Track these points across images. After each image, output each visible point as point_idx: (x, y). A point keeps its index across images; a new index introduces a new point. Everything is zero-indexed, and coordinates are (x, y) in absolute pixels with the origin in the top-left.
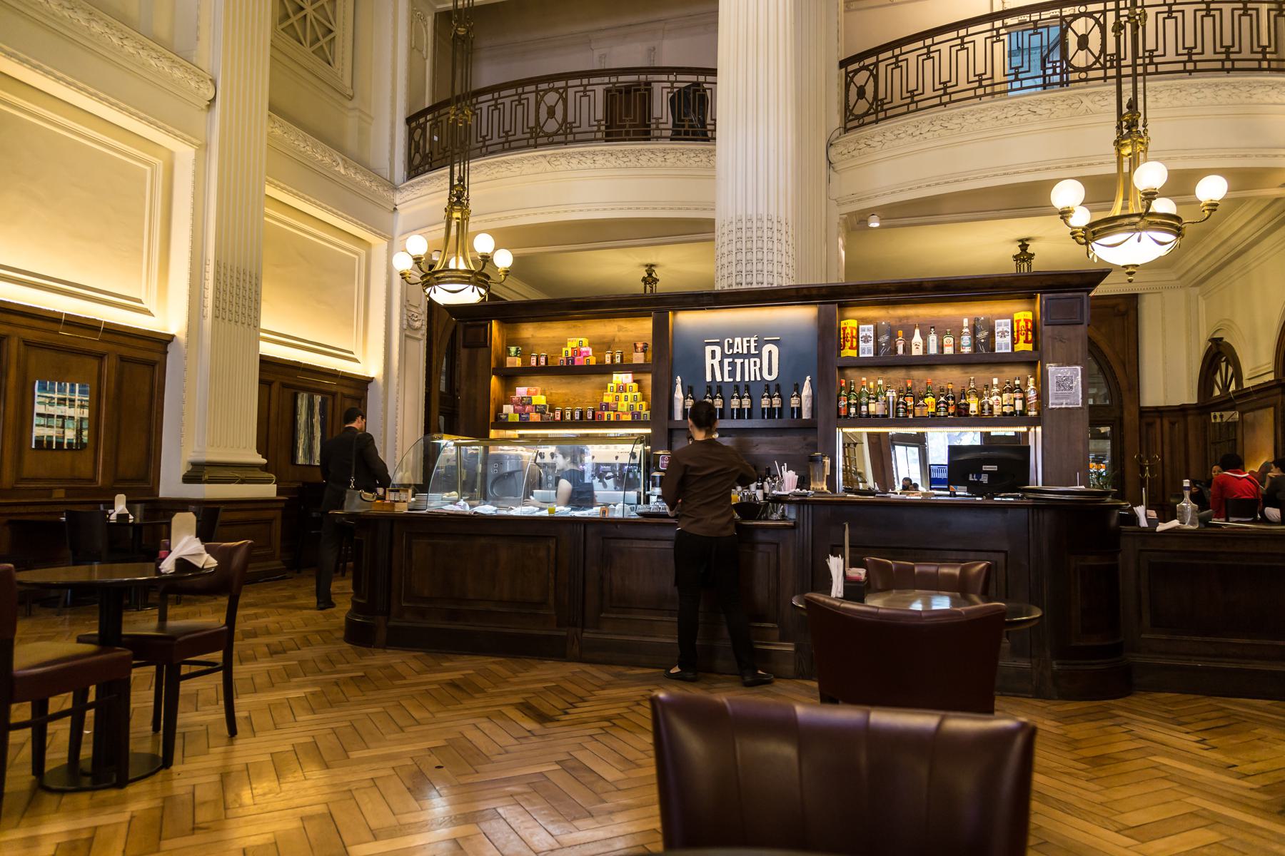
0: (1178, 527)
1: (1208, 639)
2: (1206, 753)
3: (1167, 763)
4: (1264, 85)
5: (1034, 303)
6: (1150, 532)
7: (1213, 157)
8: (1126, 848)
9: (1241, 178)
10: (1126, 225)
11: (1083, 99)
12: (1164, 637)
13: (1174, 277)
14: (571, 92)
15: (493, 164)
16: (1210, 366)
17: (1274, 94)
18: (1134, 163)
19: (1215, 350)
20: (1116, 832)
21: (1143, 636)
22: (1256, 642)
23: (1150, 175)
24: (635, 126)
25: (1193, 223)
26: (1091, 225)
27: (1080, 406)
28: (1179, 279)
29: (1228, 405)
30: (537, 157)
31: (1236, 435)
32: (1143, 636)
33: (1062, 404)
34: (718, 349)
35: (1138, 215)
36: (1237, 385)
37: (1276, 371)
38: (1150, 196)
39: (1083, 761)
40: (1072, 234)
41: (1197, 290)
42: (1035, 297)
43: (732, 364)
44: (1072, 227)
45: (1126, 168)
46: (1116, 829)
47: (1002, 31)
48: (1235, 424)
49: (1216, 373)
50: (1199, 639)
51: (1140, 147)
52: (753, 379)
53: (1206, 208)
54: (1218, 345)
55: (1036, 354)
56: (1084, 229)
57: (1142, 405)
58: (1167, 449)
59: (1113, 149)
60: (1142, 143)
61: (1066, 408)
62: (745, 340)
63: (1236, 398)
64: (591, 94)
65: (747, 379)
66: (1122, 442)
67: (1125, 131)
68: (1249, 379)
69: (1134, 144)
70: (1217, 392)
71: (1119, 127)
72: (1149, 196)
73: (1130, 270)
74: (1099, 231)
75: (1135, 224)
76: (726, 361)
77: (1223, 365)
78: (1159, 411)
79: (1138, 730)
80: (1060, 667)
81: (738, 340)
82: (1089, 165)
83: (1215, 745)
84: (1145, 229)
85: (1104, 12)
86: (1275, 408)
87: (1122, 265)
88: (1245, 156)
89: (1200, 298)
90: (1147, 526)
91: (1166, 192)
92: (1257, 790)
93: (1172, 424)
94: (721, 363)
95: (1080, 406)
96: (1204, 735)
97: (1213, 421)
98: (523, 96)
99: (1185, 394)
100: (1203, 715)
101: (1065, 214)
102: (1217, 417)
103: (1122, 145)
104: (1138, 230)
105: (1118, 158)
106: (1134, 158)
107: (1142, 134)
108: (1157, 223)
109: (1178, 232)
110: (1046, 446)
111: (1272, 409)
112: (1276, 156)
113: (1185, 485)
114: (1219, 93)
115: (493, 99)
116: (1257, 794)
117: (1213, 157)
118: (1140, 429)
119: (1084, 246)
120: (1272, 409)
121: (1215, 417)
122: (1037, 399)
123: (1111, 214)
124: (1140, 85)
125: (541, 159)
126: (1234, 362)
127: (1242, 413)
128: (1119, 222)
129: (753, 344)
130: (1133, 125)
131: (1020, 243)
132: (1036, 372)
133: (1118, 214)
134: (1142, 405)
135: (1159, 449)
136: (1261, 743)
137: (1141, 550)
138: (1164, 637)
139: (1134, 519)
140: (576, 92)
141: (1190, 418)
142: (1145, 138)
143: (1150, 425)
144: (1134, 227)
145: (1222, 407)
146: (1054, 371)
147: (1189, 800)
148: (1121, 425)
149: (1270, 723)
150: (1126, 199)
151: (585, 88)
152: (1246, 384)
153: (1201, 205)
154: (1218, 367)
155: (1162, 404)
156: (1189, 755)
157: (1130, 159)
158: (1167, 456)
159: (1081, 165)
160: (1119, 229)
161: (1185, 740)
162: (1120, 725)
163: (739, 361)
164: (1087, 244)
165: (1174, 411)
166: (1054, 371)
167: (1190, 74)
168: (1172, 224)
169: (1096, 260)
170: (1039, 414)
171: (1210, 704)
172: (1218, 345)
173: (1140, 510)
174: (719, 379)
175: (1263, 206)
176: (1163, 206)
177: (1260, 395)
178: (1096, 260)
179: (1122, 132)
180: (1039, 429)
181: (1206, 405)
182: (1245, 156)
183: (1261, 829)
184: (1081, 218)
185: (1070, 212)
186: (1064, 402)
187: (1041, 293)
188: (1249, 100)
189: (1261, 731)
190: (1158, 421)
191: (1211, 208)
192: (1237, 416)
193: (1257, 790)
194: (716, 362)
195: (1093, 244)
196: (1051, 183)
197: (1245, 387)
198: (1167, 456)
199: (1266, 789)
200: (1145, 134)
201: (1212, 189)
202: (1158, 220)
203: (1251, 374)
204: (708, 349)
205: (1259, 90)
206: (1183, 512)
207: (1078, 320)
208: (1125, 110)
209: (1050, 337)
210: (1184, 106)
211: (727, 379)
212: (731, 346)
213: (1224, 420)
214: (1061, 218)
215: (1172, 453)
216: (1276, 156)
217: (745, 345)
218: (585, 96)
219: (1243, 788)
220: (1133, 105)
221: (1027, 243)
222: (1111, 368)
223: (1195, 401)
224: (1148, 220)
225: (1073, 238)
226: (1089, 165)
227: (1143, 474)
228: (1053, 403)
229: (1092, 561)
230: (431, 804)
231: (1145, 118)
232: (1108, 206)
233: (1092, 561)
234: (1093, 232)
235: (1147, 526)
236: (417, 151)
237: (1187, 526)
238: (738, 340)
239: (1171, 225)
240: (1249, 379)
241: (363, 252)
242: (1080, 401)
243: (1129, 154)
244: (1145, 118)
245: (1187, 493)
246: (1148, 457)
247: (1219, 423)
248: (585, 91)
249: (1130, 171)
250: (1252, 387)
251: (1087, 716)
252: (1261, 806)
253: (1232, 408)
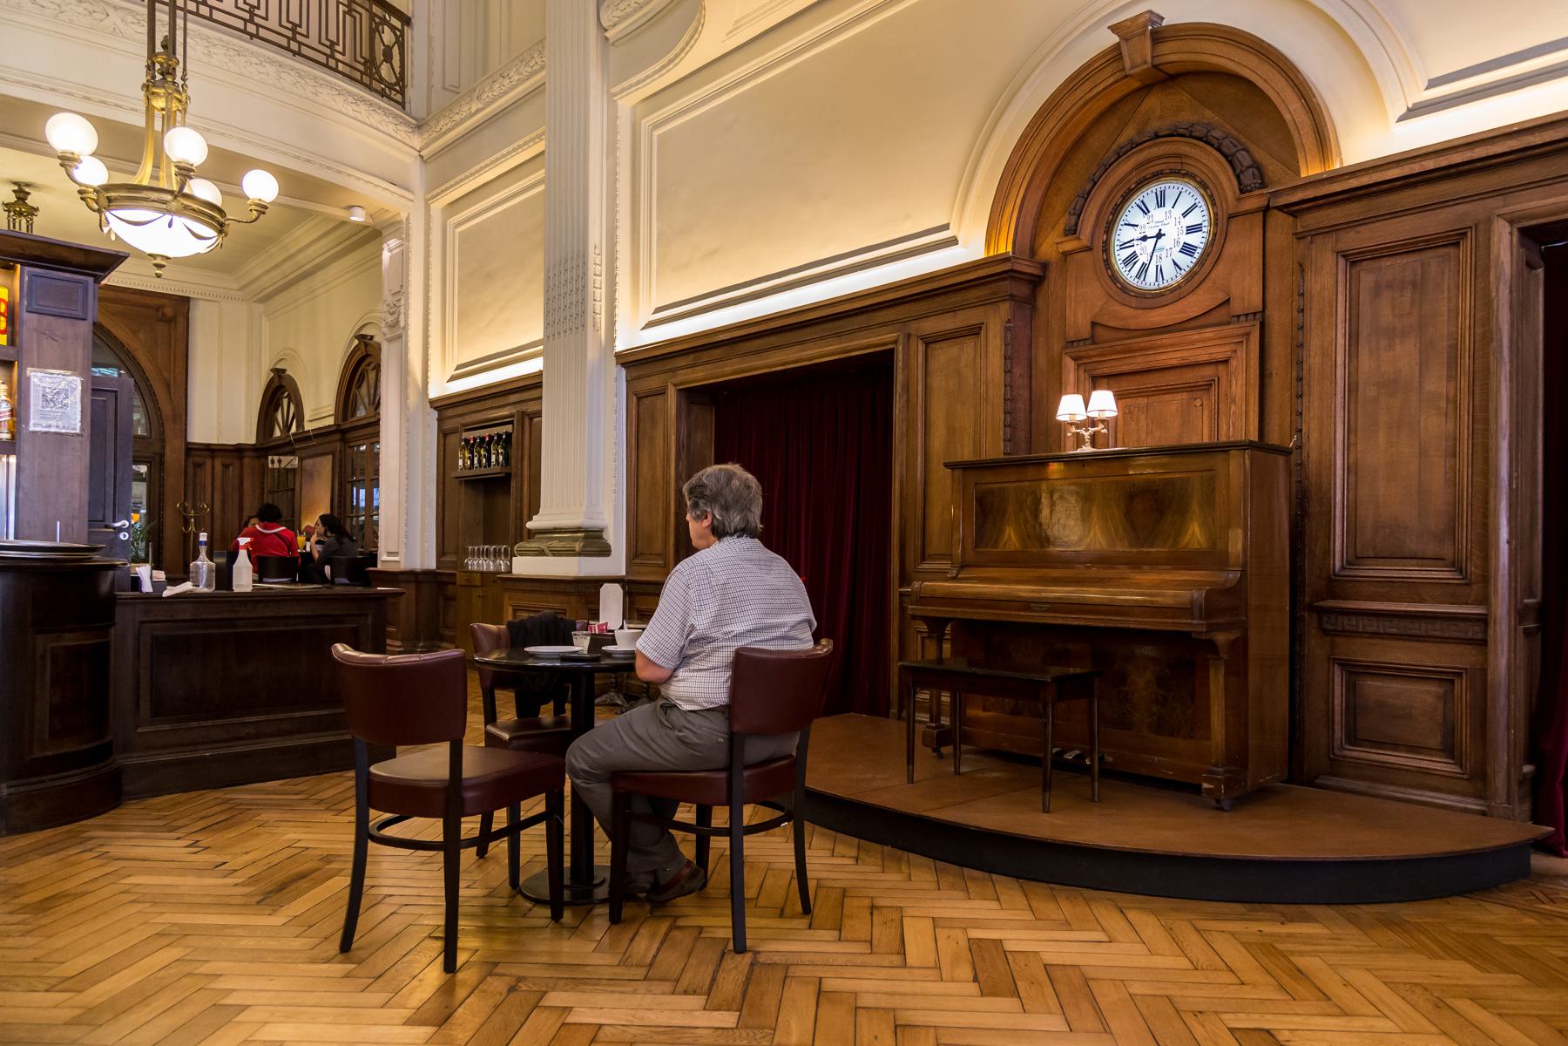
0: (191, 591)
1: (218, 722)
2: (193, 857)
3: (140, 882)
4: (332, 87)
5: (13, 276)
6: (155, 599)
7: (274, 150)
8: (55, 1007)
9: (296, 184)
10: (154, 201)
11: (110, 11)
12: (166, 727)
13: (236, 287)
16: (270, 402)
17: (340, 99)
18: (169, 121)
19: (276, 383)
20: (47, 991)
21: (139, 730)
22: (272, 717)
23: (186, 145)
25: (239, 221)
26: (107, 188)
27: (78, 431)
28: (240, 289)
29: (288, 449)
31: (294, 484)
32: (139, 730)
33: (50, 426)
35: (171, 192)
36: (298, 427)
37: (336, 415)
38: (185, 172)
39: (22, 911)
40: (80, 192)
41: (261, 308)
42: (12, 268)
44: (80, 185)
45: (158, 125)
46: (46, 987)
48: (294, 470)
49: (277, 410)
50: (209, 723)
51: (175, 105)
53: (253, 207)
54: (280, 377)
55: (12, 351)
56: (96, 191)
57: (189, 440)
58: (217, 496)
59: (141, 94)
60: (180, 101)
61: (56, 433)
63: (297, 441)
66: (162, 486)
67: (158, 77)
68: (311, 421)
69: (168, 96)
70: (277, 433)
71: (150, 67)
72: (184, 172)
73: (159, 261)
74: (116, 199)
75: (165, 202)
77: (285, 401)
78: (210, 450)
79: (114, 850)
80: (12, 790)
82: (116, 105)
83: (207, 845)
84: (177, 213)
86: (334, 456)
87: (148, 252)
88: (309, 161)
89: (263, 317)
90: (152, 590)
91: (205, 172)
92: (243, 884)
93: (226, 466)
95: (78, 431)
96: (195, 837)
97: (270, 466)
99: (243, 432)
100: (203, 814)
101: (67, 161)
102: (275, 462)
103: (153, 93)
104: (168, 212)
105: (147, 108)
106: (169, 117)
107: (181, 89)
108: (194, 210)
109: (221, 228)
110: (23, 483)
111: (330, 457)
112: (340, 172)
113: (201, 539)
114: (283, 75)
116: (242, 888)
117: (274, 150)
118: (186, 471)
119: (97, 214)
120: (330, 457)
121: (273, 462)
122: (12, 415)
123: (135, 181)
124: (180, 22)
126: (297, 400)
127: (301, 460)
128: (145, 194)
130: (168, 72)
131: (16, 188)
132: (11, 377)
133: (145, 183)
134: (189, 440)
135: (208, 496)
136: (261, 829)
137: (144, 622)
138: (166, 727)
139: (136, 582)
141: (246, 461)
142: (184, 95)
143: (198, 466)
144: (164, 206)
145: (281, 450)
146: (40, 380)
147: (158, 920)
148: (162, 463)
149: (279, 805)
150: (156, 166)
152: (308, 427)
153: (249, 202)
154: (279, 405)
155: (215, 442)
156: (172, 865)
157: (163, 115)
158: (217, 505)
159: (104, 102)
160: (145, 204)
161: (172, 847)
162: (91, 850)
164: (99, 211)
165: (232, 451)
166: (40, 380)
167: (252, 39)
168: (214, 216)
169: (113, 238)
170: (13, 437)
171: (215, 798)
172: (280, 377)
173: (144, 571)
175: (330, 226)
176: (204, 190)
177: (320, 440)
178: (113, 238)
179: (154, 77)
180: (13, 459)
181: (265, 447)
182: (309, 161)
183: (233, 927)
184: (94, 173)
185: (74, 160)
186: (53, 423)
187: (22, 264)
188: (312, 97)
189: (264, 816)
190: (209, 462)
191: (259, 209)
192: (296, 462)
193: (243, 884)
195: (107, 214)
196: (53, 110)
197: (306, 429)
198: (217, 505)
199: (253, 880)
200: (185, 91)
201: (261, 186)
202: (196, 206)
203: (312, 416)
205: (326, 91)
206: (197, 573)
207: (79, 313)
208: (159, 49)
209: (34, 329)
210: (242, 75)
213: (283, 466)
214: (61, 165)
215: (223, 503)
216: (340, 172)
219: (226, 885)
220: (169, 45)
221: (27, 190)
222: (150, 387)
223: (252, 440)
224: (179, 202)
225: (82, 199)
226: (116, 105)
227: (186, 529)
228: (36, 424)
229: (70, 640)
231: (185, 69)
232: (132, 169)
233: (70, 640)
234: (107, 198)
235: (152, 590)
237: (202, 589)
239: (212, 217)
240: (311, 421)
242: (79, 425)
243: (163, 109)
244: (185, 69)
245: (203, 549)
246: (194, 507)
247: (278, 469)
249: (163, 130)
250: (312, 430)
251: (45, 849)
252: (243, 901)
253: (292, 453)
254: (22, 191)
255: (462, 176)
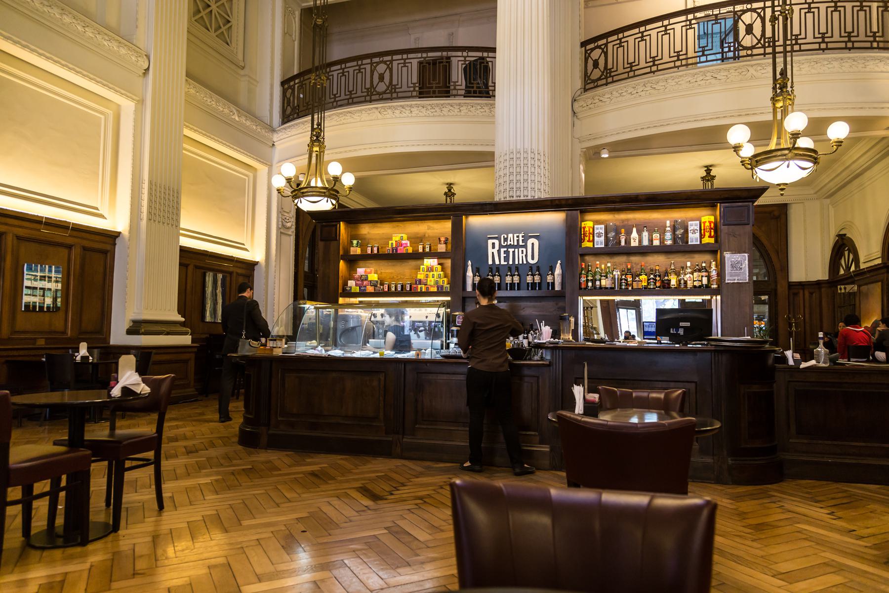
0: (815, 365)
1: (835, 443)
2: (834, 522)
3: (808, 529)
4: (874, 59)
5: (715, 210)
6: (796, 369)
7: (839, 108)
8: (779, 587)
9: (859, 124)
10: (779, 156)
11: (749, 68)
12: (805, 441)
13: (812, 192)
14: (395, 64)
15: (341, 113)
16: (837, 254)
17: (881, 65)
18: (785, 113)
19: (840, 242)
20: (772, 576)
21: (791, 440)
22: (869, 444)
23: (796, 121)
24: (439, 87)
25: (826, 154)
26: (755, 156)
27: (747, 281)
28: (816, 193)
29: (850, 280)
30: (372, 109)
31: (855, 301)
32: (791, 440)
33: (735, 280)
34: (497, 242)
35: (788, 149)
36: (856, 267)
37: (883, 257)
38: (795, 136)
39: (749, 527)
40: (741, 162)
41: (828, 201)
42: (716, 206)
43: (507, 252)
44: (742, 158)
45: (779, 117)
46: (772, 575)
47: (693, 22)
48: (854, 294)
49: (841, 258)
50: (829, 442)
51: (788, 102)
52: (521, 262)
53: (834, 144)
54: (843, 239)
55: (717, 245)
56: (750, 159)
57: (790, 281)
58: (807, 311)
59: (770, 104)
60: (790, 99)
61: (737, 283)
62: (515, 235)
63: (855, 275)
64: (409, 65)
65: (517, 263)
66: (776, 306)
67: (779, 91)
68: (864, 263)
69: (784, 100)
70: (842, 272)
71: (774, 88)
72: (795, 136)
73: (782, 187)
74: (760, 160)
75: (785, 155)
76: (503, 250)
77: (846, 253)
78: (802, 285)
79: (787, 506)
80: (733, 462)
81: (510, 236)
82: (753, 114)
83: (840, 516)
84: (792, 159)
85: (764, 9)
86: (882, 282)
87: (776, 183)
88: (862, 108)
89: (830, 206)
90: (793, 364)
91: (807, 133)
92: (870, 547)
93: (811, 294)
94: (499, 251)
95: (747, 281)
96: (833, 510)
97: (839, 291)
98: (362, 67)
99: (820, 273)
100: (833, 496)
101: (737, 148)
102: (842, 289)
103: (776, 100)
104: (787, 159)
105: (774, 109)
106: (785, 110)
107: (790, 93)
108: (800, 155)
109: (815, 161)
110: (724, 309)
111: (880, 283)
112: (883, 108)
113: (820, 336)
114: (844, 64)
115: (341, 69)
116: (870, 550)
117: (839, 108)
118: (789, 297)
119: (750, 171)
120: (880, 283)
121: (841, 289)
122: (718, 276)
123: (768, 148)
124: (789, 59)
125: (374, 110)
126: (854, 251)
127: (859, 286)
128: (774, 154)
129: (521, 239)
130: (784, 86)
131: (706, 169)
132: (716, 258)
133: (773, 148)
134: (790, 281)
135: (802, 311)
136: (873, 515)
137: (790, 381)
138: (805, 441)
139: (784, 359)
140: (398, 64)
141: (823, 290)
142: (792, 96)
143: (796, 294)
144: (785, 157)
145: (845, 282)
146: (729, 257)
147: (823, 554)
148: (776, 294)
149: (879, 501)
150: (779, 138)
151: (405, 61)
152: (862, 266)
153: (831, 142)
154: (843, 255)
155: (804, 280)
156: (823, 523)
157: (782, 110)
158: (807, 316)
159: (748, 115)
160: (774, 159)
161: (820, 513)
162: (775, 502)
163: (511, 250)
164: (752, 169)
165: (812, 284)
166: (729, 257)
167: (823, 52)
168: (811, 155)
169: (758, 180)
170: (719, 287)
171: (837, 488)
172: (843, 239)
173: (789, 353)
174: (497, 262)
175: (874, 143)
176: (805, 142)
177: (872, 274)
178: (758, 180)
179: (776, 92)
180: (719, 297)
181: (834, 280)
182: (862, 108)
183: (873, 574)
184: (748, 151)
185: (740, 147)
186: (736, 278)
187: (720, 203)
188: (864, 69)
189: (872, 506)
190: (801, 292)
191: (838, 144)
192: (856, 288)
193: (870, 547)
194: (495, 251)
195: (756, 169)
196: (727, 127)
197: (861, 268)
198: (807, 316)
199: (876, 547)
200: (792, 93)
201: (838, 131)
202: (801, 153)
203: (865, 259)
204: (490, 242)
205: (871, 63)
206: (818, 355)
207: (746, 222)
208: (778, 76)
209: (726, 233)
210: (819, 73)
211: (503, 263)
212: (506, 240)
213: (847, 291)
214: (734, 151)
215: (811, 314)
216: (883, 108)
217: (516, 239)
218: (405, 66)
219: (860, 546)
220: (784, 73)
221: (711, 168)
222: (768, 255)
223: (826, 278)
224: (794, 153)
225: (743, 165)
226: (753, 114)
227: (791, 329)
228: (728, 279)
229: (755, 388)
230: (298, 557)
231: (792, 82)
232: (767, 143)
233: (755, 388)
234: (756, 161)
235: (793, 364)
236: (289, 105)
237: (822, 365)
238: (510, 236)
239: (810, 156)
240: (864, 263)
241: (251, 175)
242: (747, 278)
243: (781, 107)
244: (792, 82)
245: (821, 342)
246: (794, 317)
247: (843, 293)
248: (405, 63)
249: (782, 118)
250: (866, 268)
251: (752, 496)
252: (873, 558)
253: (853, 283)
254: (708, 169)
255: (220, 140)
